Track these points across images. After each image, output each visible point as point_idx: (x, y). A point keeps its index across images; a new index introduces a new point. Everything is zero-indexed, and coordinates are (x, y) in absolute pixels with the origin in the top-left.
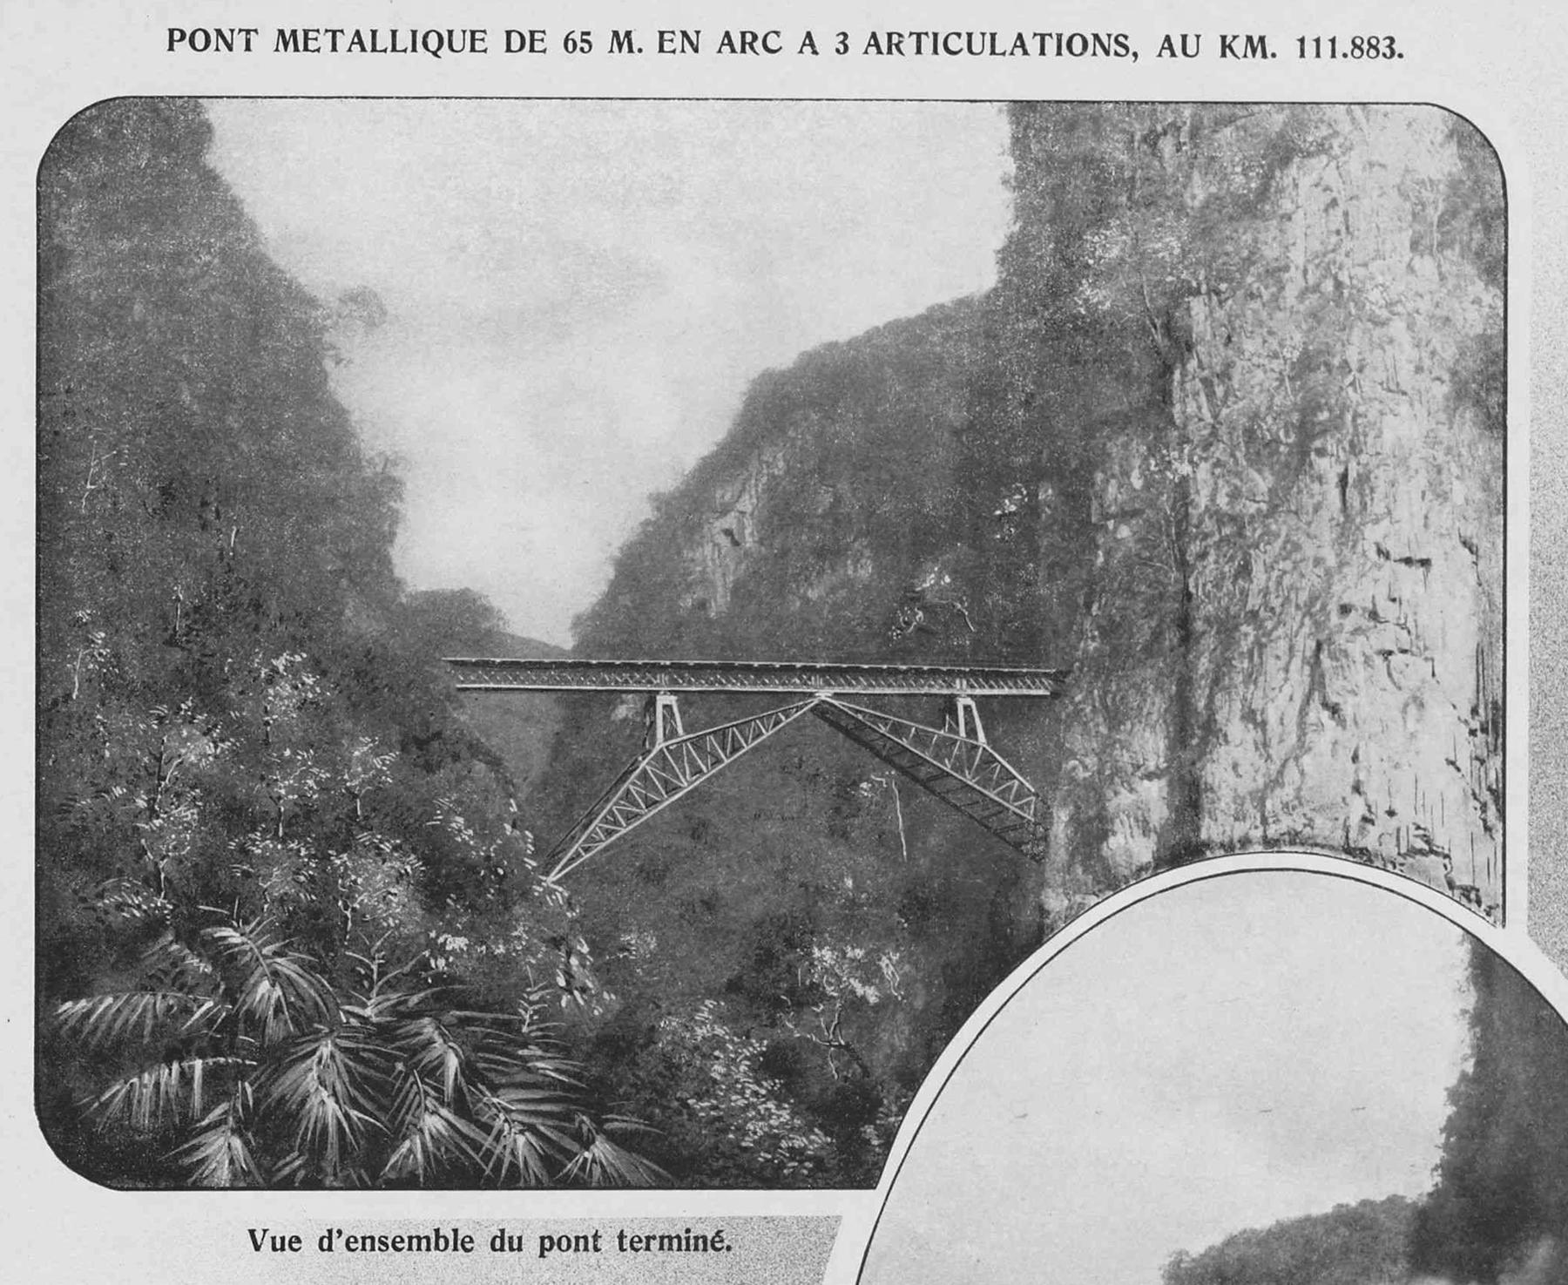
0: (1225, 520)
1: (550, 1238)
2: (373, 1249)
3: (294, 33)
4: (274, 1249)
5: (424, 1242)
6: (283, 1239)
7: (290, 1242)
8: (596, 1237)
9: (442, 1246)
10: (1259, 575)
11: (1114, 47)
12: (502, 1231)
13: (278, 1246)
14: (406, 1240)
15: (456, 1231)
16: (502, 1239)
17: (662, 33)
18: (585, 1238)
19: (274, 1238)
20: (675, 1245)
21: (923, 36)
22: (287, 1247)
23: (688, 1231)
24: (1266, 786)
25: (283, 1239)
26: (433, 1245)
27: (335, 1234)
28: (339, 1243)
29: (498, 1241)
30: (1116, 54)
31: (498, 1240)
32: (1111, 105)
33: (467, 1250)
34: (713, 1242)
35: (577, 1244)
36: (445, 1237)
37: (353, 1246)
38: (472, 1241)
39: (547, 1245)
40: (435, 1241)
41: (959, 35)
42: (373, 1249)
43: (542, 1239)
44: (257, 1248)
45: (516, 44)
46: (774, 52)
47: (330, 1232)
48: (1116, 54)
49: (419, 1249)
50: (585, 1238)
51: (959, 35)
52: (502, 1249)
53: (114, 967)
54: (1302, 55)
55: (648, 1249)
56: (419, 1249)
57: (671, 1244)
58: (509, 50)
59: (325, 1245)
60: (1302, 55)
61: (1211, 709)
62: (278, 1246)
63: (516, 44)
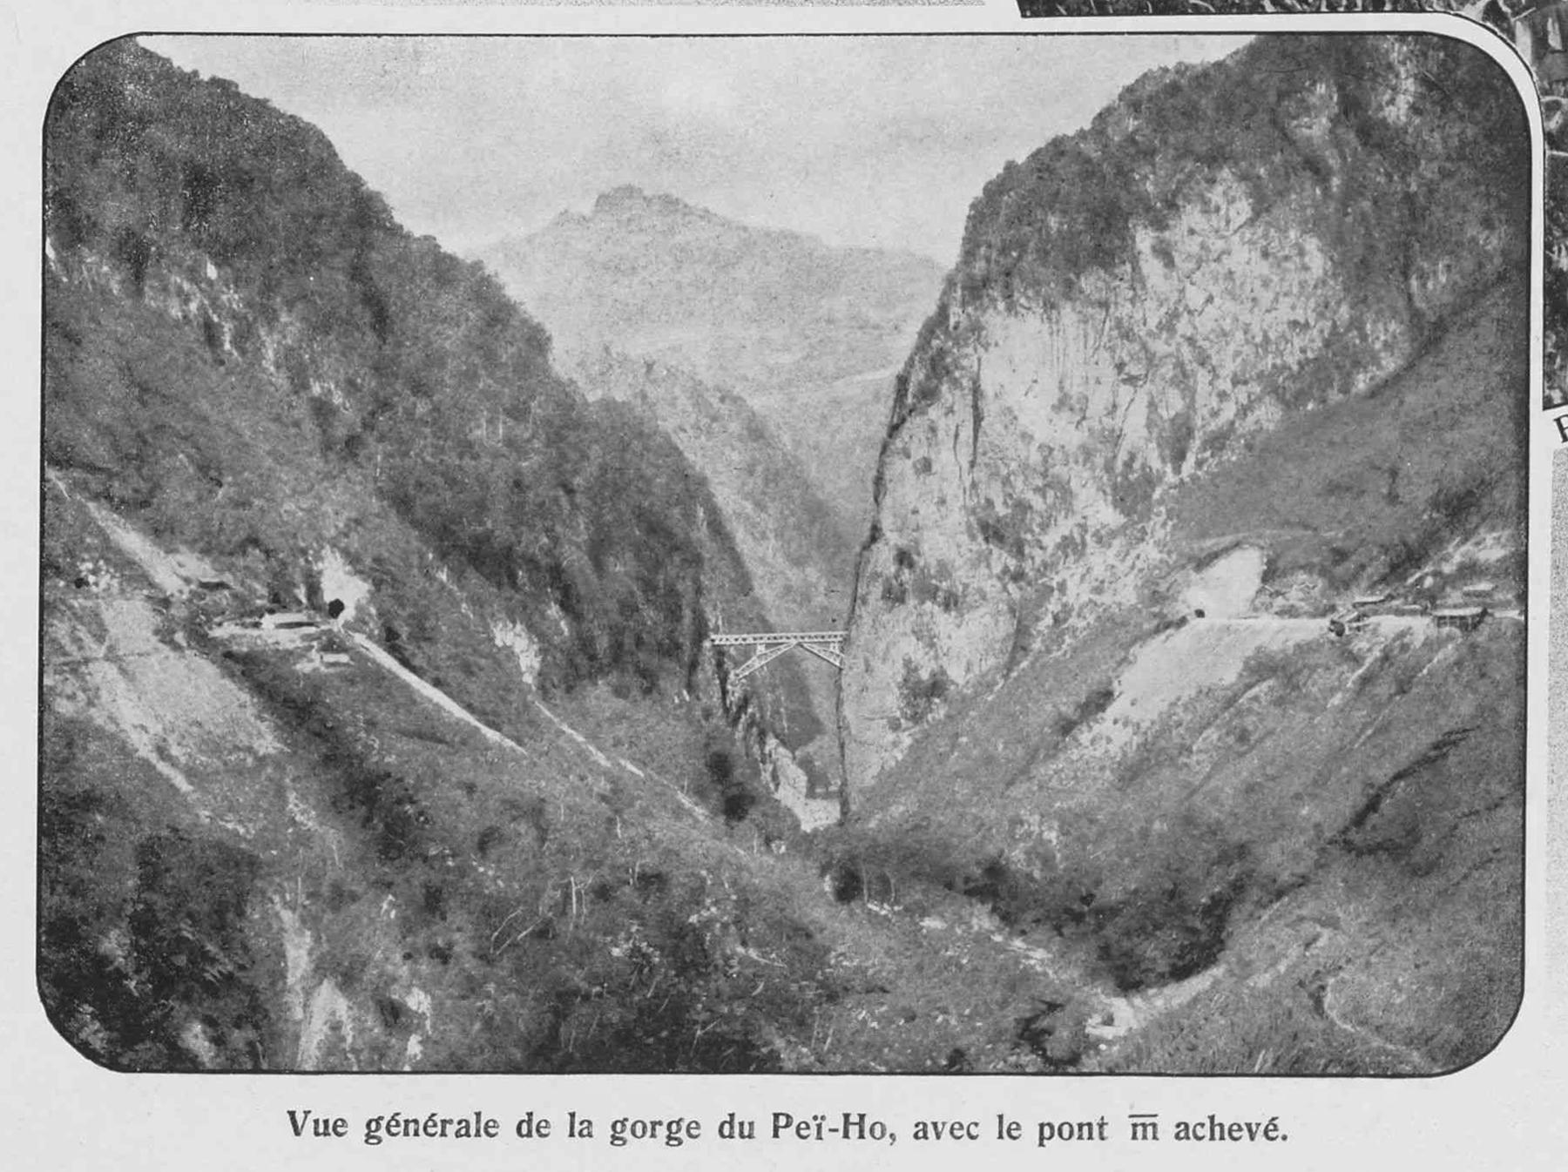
4: (317, 1134)
6: (326, 1122)
7: (1230, 1131)
12: (732, 1115)
15: (478, 1115)
16: (731, 1123)
18: (1090, 1125)
19: (316, 1122)
29: (525, 1126)
31: (727, 1126)
32: (84, 63)
34: (1230, 1131)
35: (326, 1127)
37: (803, 1133)
40: (433, 1127)
43: (750, 1136)
44: (297, 1133)
49: (1145, 1137)
50: (1090, 1125)
52: (731, 1136)
55: (443, 1134)
56: (1145, 1137)
57: (1145, 1131)
61: (1379, 146)
62: (321, 1130)
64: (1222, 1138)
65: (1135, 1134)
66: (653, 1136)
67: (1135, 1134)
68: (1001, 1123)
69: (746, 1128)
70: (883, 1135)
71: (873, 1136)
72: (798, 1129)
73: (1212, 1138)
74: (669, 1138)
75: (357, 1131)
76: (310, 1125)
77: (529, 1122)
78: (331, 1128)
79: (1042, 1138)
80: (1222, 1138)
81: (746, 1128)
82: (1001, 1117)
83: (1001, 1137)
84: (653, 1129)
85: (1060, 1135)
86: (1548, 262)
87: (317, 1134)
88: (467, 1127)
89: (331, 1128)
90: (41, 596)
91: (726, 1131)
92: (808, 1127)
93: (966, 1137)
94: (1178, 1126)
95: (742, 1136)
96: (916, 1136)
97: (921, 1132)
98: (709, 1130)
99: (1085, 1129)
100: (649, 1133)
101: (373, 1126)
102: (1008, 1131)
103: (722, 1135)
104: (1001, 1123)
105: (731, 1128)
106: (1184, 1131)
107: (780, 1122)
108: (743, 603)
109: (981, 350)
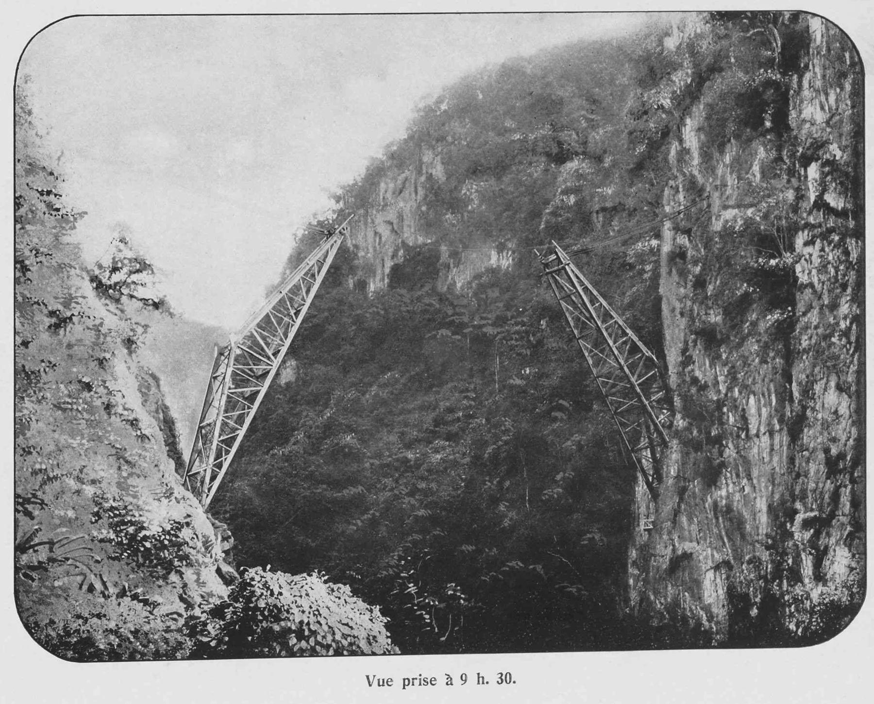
0: (431, 439)
1: (408, 680)
4: (379, 685)
6: (383, 680)
7: (387, 682)
10: (709, 587)
13: (381, 683)
19: (379, 680)
22: (385, 684)
23: (420, 675)
24: (711, 612)
25: (383, 680)
38: (435, 680)
39: (407, 682)
43: (404, 680)
44: (370, 685)
53: (135, 497)
62: (381, 683)
65: (479, 681)
66: (413, 685)
67: (479, 681)
70: (510, 682)
75: (398, 683)
76: (376, 683)
78: (385, 683)
79: (404, 685)
85: (506, 681)
87: (379, 685)
89: (385, 683)
90: (15, 254)
96: (447, 684)
100: (411, 683)
109: (810, 105)
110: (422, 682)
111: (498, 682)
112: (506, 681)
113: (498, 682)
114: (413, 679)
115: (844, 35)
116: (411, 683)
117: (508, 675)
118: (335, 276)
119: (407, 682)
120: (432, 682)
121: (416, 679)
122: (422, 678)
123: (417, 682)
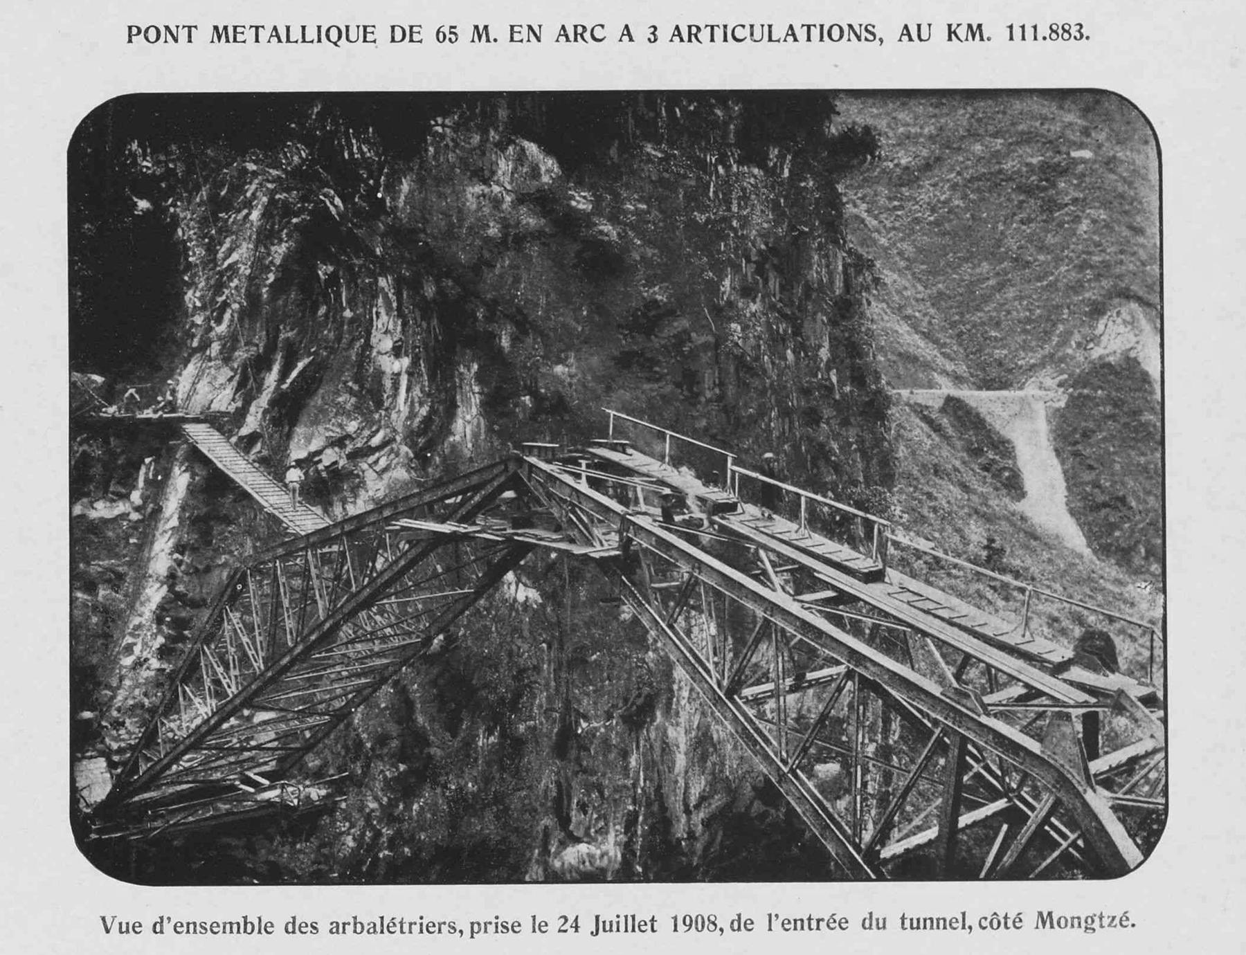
1: (479, 924)
2: (195, 932)
3: (225, 28)
5: (235, 927)
6: (128, 924)
7: (134, 927)
8: (653, 920)
9: (249, 930)
11: (864, 34)
13: (124, 929)
14: (185, 925)
15: (260, 919)
17: (512, 27)
20: (235, 929)
21: (193, 29)
23: (421, 918)
25: (128, 924)
26: (242, 930)
27: (774, 918)
28: (168, 927)
30: (866, 39)
33: (136, 932)
35: (128, 927)
36: (252, 923)
37: (178, 929)
41: (743, 26)
42: (195, 932)
43: (472, 924)
44: (108, 931)
45: (398, 36)
46: (600, 40)
47: (162, 918)
48: (866, 39)
51: (743, 26)
54: (675, 930)
57: (231, 928)
58: (393, 40)
59: (158, 929)
60: (675, 930)
62: (124, 929)
63: (398, 36)
64: (945, 928)
66: (486, 931)
68: (534, 920)
69: (1076, 924)
71: (1060, 926)
72: (175, 926)
73: (188, 932)
74: (1086, 928)
76: (115, 928)
77: (294, 923)
80: (945, 928)
81: (1076, 924)
82: (534, 917)
83: (534, 931)
84: (344, 928)
85: (703, 918)
86: (704, 549)
87: (121, 932)
88: (338, 927)
91: (867, 925)
92: (646, 924)
93: (838, 928)
94: (332, 924)
95: (912, 928)
96: (331, 931)
97: (1018, 921)
98: (279, 929)
99: (799, 923)
100: (1069, 924)
101: (1089, 921)
102: (539, 927)
103: (287, 931)
104: (534, 920)
105: (872, 923)
106: (337, 928)
107: (1046, 919)
108: (965, 556)
110: (500, 928)
111: (649, 40)
112: (703, 918)
113: (649, 40)
114: (344, 924)
115: (1163, 824)
116: (1069, 924)
117: (700, 918)
118: (669, 213)
119: (476, 928)
120: (514, 928)
121: (490, 923)
122: (500, 921)
123: (491, 928)
